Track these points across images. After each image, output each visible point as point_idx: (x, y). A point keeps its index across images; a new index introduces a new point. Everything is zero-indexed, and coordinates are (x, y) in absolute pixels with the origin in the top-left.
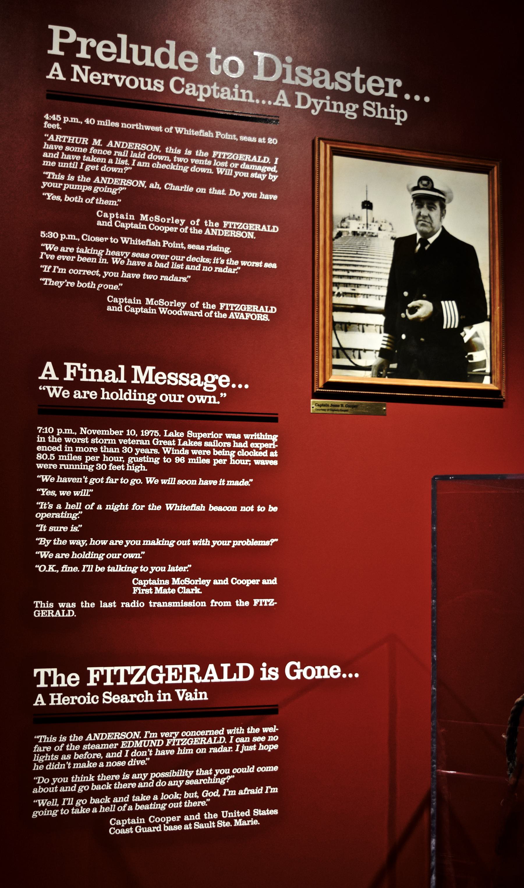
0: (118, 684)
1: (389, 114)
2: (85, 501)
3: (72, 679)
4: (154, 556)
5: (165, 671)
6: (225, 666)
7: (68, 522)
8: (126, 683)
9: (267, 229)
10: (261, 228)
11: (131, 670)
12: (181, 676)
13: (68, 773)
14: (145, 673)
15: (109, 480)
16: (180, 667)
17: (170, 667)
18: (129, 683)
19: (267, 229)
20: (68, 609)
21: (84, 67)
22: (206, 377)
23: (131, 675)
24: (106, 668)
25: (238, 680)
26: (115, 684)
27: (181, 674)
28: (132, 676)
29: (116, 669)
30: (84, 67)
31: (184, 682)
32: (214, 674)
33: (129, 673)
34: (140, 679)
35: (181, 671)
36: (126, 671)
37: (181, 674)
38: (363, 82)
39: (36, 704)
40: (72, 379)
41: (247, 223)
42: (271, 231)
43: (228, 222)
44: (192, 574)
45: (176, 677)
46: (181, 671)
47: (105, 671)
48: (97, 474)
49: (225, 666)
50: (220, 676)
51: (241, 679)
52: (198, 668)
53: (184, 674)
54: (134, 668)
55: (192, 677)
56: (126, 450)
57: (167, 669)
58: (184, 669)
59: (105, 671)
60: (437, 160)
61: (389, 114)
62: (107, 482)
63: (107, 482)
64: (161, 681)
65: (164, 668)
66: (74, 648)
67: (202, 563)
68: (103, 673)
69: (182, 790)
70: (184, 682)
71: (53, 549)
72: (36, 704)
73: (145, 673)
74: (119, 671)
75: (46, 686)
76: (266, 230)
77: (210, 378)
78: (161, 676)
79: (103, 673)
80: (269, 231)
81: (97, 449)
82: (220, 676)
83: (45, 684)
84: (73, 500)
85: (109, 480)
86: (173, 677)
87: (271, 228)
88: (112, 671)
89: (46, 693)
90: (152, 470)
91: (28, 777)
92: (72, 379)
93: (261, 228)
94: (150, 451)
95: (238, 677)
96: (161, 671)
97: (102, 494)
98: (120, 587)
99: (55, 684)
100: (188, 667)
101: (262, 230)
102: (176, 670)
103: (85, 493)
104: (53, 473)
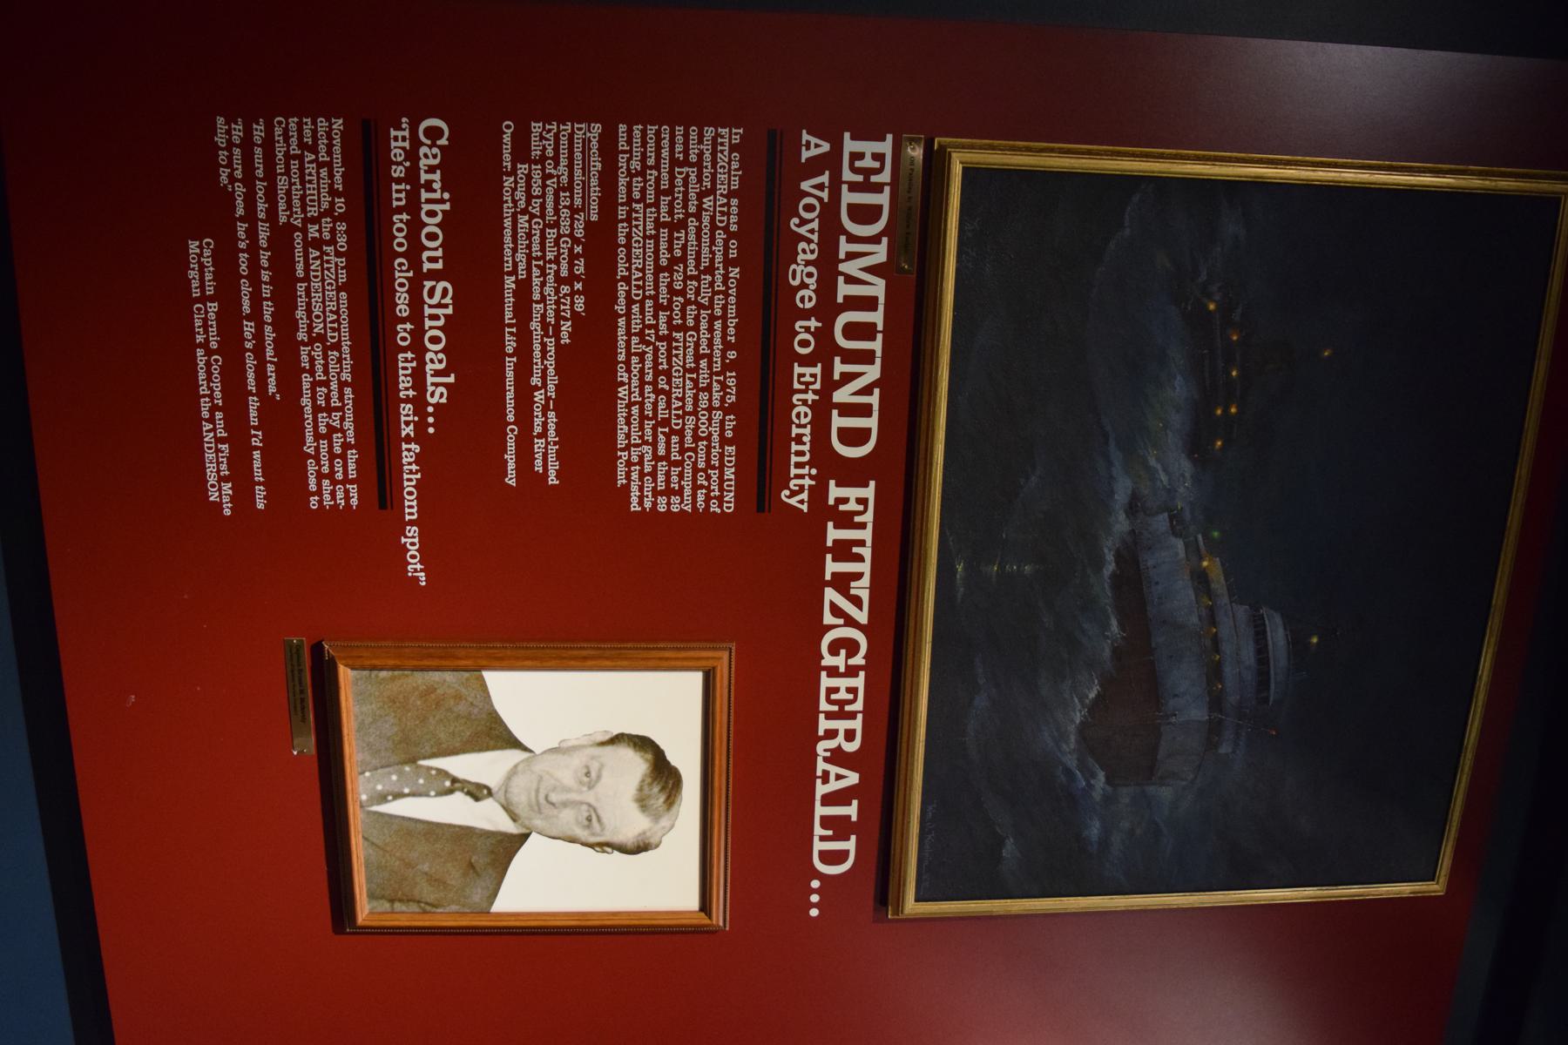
0: (829, 557)
1: (799, 465)
5: (852, 672)
6: (852, 811)
8: (828, 577)
11: (861, 588)
12: (860, 178)
14: (850, 622)
15: (409, 450)
16: (859, 706)
17: (859, 682)
18: (829, 584)
21: (877, 391)
22: (811, 269)
23: (849, 588)
24: (870, 527)
25: (816, 839)
26: (829, 550)
27: (867, 179)
28: (844, 590)
29: (866, 552)
30: (877, 391)
31: (845, 187)
32: (834, 785)
33: (853, 584)
34: (836, 611)
35: (874, 179)
36: (859, 576)
37: (867, 179)
38: (805, 402)
39: (805, 137)
40: (831, 502)
45: (858, 164)
46: (874, 179)
47: (863, 526)
49: (852, 811)
50: (828, 800)
51: (818, 846)
52: (851, 747)
53: (842, 715)
54: (865, 595)
55: (831, 734)
57: (857, 675)
58: (852, 716)
59: (863, 526)
61: (799, 465)
62: (404, 446)
63: (404, 446)
64: (828, 660)
65: (859, 668)
68: (857, 519)
70: (822, 716)
72: (805, 137)
73: (850, 622)
74: (860, 558)
75: (828, 577)
77: (810, 275)
78: (839, 661)
79: (857, 519)
81: (808, 305)
82: (828, 800)
83: (833, 574)
85: (409, 450)
86: (861, 156)
88: (862, 543)
92: (831, 502)
94: (431, 170)
95: (823, 839)
96: (851, 662)
100: (857, 724)
102: (877, 165)
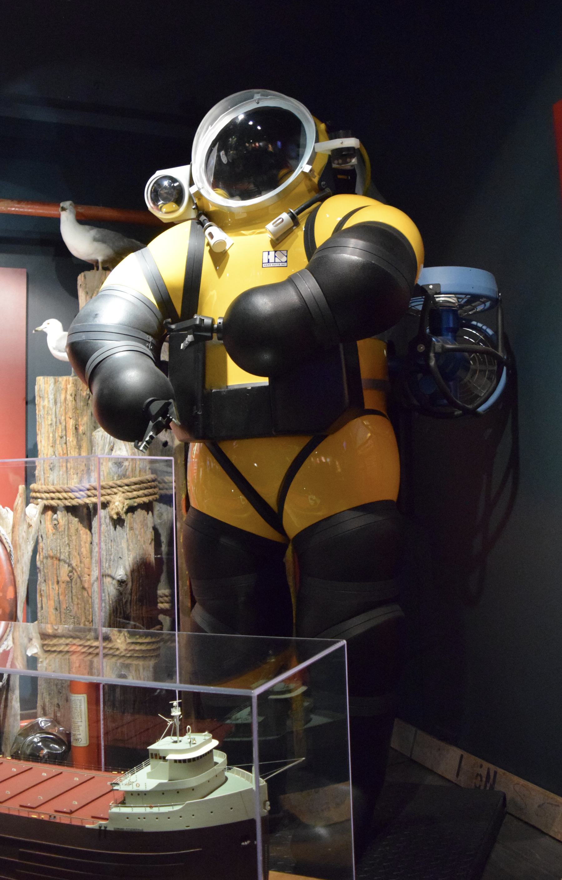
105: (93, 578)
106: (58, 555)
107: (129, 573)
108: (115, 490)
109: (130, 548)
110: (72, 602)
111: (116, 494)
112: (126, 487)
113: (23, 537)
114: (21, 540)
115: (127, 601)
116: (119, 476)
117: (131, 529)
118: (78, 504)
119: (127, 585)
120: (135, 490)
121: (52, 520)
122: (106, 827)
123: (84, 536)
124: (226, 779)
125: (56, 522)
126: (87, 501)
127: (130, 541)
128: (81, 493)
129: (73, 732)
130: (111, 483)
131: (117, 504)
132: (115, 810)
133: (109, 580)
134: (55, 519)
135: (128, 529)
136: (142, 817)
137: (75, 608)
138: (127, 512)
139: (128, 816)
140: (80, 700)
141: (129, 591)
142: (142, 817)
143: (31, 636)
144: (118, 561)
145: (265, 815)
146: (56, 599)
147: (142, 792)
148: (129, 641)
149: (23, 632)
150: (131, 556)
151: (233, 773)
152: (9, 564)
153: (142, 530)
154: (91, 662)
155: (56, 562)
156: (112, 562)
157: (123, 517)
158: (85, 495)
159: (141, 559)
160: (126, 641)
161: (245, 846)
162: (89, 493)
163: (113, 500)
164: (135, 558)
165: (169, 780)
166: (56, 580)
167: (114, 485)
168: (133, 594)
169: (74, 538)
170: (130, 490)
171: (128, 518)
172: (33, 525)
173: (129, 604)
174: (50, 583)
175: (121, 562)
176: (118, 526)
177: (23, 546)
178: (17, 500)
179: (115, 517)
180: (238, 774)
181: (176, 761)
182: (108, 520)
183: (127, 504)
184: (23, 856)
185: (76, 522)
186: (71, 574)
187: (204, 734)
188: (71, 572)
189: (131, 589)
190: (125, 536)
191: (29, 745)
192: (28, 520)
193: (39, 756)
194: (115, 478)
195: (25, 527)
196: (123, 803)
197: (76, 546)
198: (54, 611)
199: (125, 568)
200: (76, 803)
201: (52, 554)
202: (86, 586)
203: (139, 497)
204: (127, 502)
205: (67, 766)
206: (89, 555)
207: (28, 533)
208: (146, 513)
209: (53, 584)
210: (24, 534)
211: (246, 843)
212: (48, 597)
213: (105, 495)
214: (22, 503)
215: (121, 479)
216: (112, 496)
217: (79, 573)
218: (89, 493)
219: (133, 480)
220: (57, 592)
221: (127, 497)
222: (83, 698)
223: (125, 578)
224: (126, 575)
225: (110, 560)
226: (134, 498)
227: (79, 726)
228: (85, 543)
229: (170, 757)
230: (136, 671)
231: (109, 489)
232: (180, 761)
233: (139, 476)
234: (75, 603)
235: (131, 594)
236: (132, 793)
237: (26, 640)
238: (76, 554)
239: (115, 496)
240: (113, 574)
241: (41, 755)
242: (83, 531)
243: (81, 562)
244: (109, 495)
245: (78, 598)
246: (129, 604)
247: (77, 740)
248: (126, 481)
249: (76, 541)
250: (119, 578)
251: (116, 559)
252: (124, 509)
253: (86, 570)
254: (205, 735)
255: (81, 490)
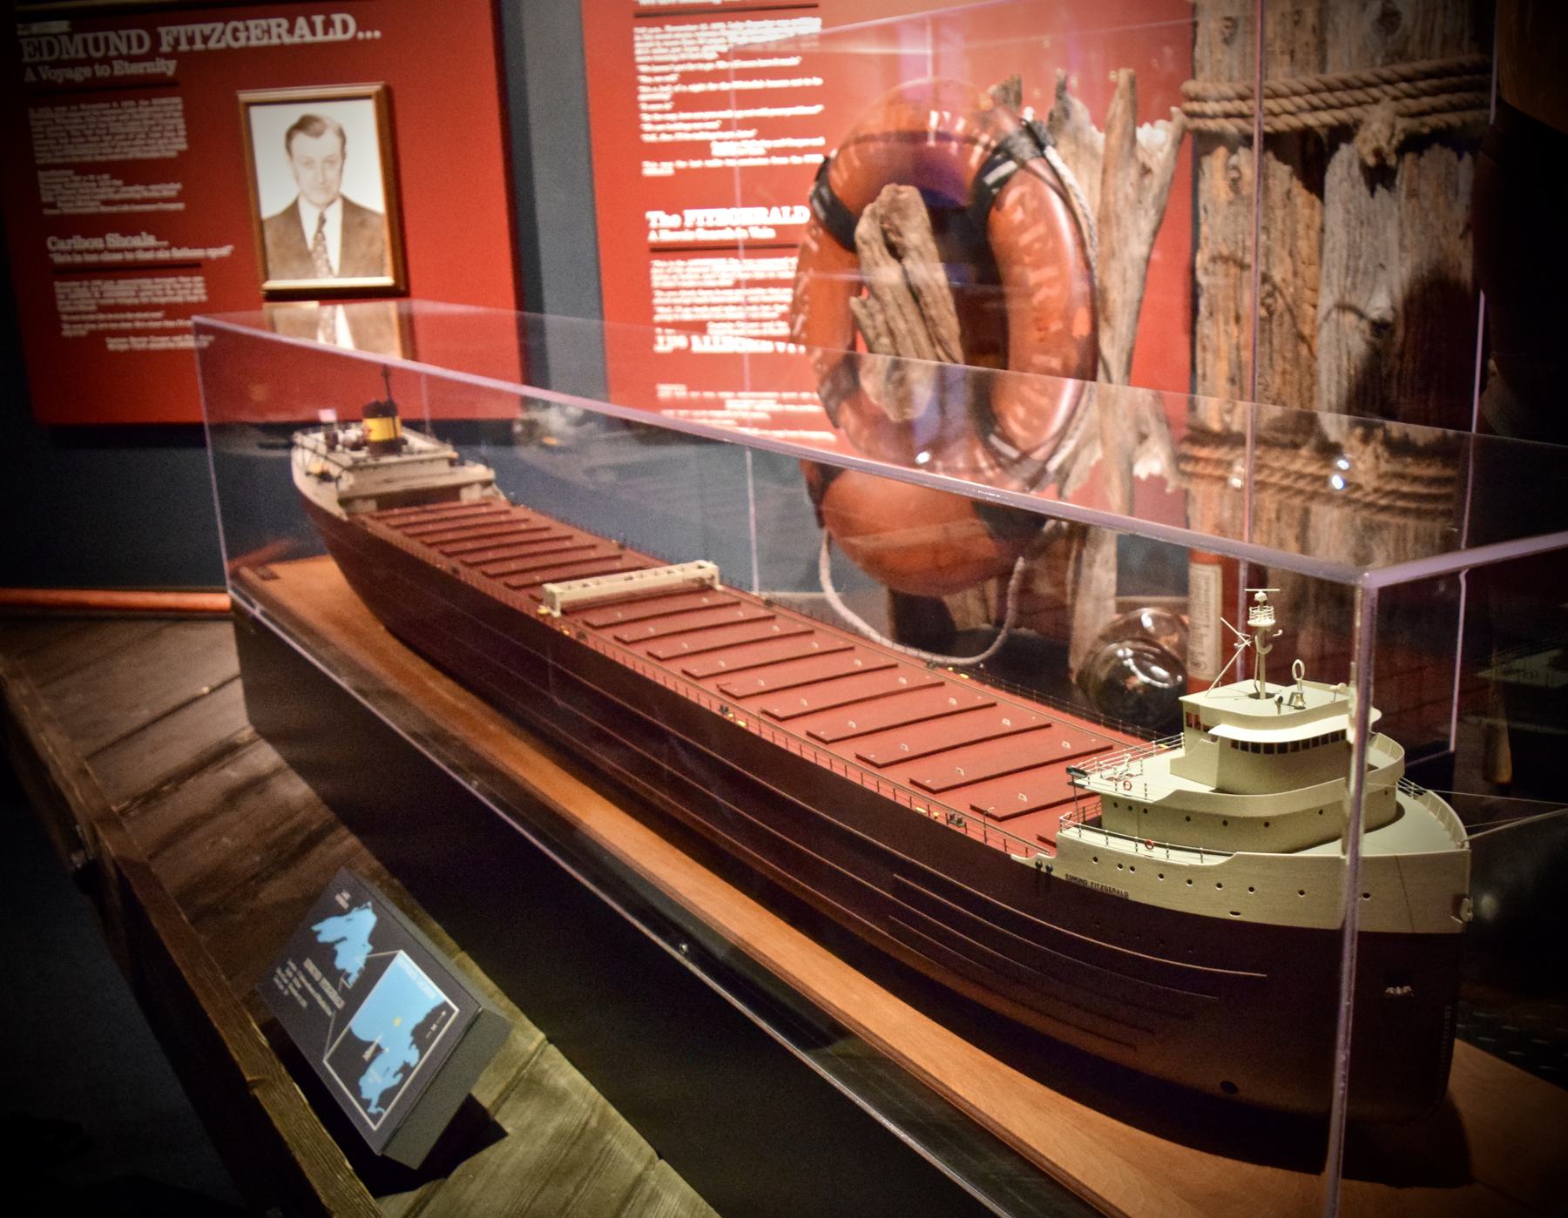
2: (674, 84)
3: (675, 220)
4: (726, 125)
7: (661, 102)
9: (313, 33)
10: (291, 31)
13: (677, 289)
14: (223, 33)
19: (313, 33)
20: (666, 169)
34: (219, 41)
41: (239, 20)
42: (331, 37)
43: (174, 29)
44: (757, 138)
48: (681, 62)
56: (701, 41)
60: (303, 645)
66: (675, 196)
67: (766, 129)
69: (759, 304)
71: (654, 123)
73: (223, 33)
76: (309, 38)
80: (320, 37)
84: (664, 84)
87: (328, 25)
89: (657, 230)
90: (723, 56)
91: (648, 292)
93: (291, 31)
97: (686, 78)
98: (702, 149)
99: (662, 225)
101: (296, 39)
103: (673, 78)
104: (649, 64)
105: (1322, 311)
106: (1240, 254)
107: (1399, 307)
108: (1375, 92)
109: (1407, 242)
110: (1272, 366)
111: (1376, 101)
112: (1404, 86)
113: (1126, 197)
114: (1121, 203)
115: (1389, 375)
116: (1387, 54)
117: (1413, 194)
118: (1287, 129)
119: (1393, 333)
120: (1425, 93)
121: (1228, 168)
122: (1049, 869)
123: (1307, 212)
124: (1400, 812)
125: (1234, 174)
126: (1310, 120)
127: (1407, 224)
128: (1298, 100)
129: (1191, 647)
130: (1366, 75)
131: (1375, 126)
132: (1072, 834)
133: (1350, 318)
134: (1235, 168)
135: (1403, 194)
136: (1127, 865)
137: (1278, 380)
138: (1401, 151)
139: (1096, 855)
140: (1207, 579)
141: (1396, 349)
142: (1127, 865)
143: (1144, 429)
144: (1375, 275)
145: (1458, 931)
146: (1234, 356)
147: (1138, 803)
148: (1384, 467)
149: (1125, 417)
150: (1408, 264)
151: (1425, 803)
152: (1079, 254)
153: (1441, 200)
154: (1306, 512)
155: (1234, 270)
156: (1360, 277)
157: (1392, 161)
158: (1306, 106)
159: (1430, 271)
160: (1377, 467)
161: (1394, 997)
162: (1315, 100)
163: (1367, 118)
164: (1418, 267)
165: (1219, 790)
166: (1232, 314)
167: (1373, 79)
168: (1408, 357)
169: (1279, 213)
170: (1413, 92)
171: (1406, 170)
172: (1156, 169)
173: (1394, 381)
174: (1221, 318)
175: (1382, 276)
176: (1379, 187)
177: (1127, 218)
178: (1113, 106)
179: (1371, 161)
180: (1434, 807)
181: (1235, 744)
182: (1356, 171)
183: (1404, 130)
184: (899, 889)
185: (1286, 177)
186: (1269, 301)
187: (1333, 687)
188: (1270, 295)
189: (1404, 344)
190: (1395, 210)
191: (1106, 662)
192: (1141, 156)
193: (1125, 688)
194: (1379, 61)
195: (1133, 172)
196: (1096, 824)
197: (1283, 234)
198: (1228, 386)
199: (1391, 292)
200: (1025, 799)
201: (1225, 252)
202: (1306, 331)
203: (1435, 110)
204: (1402, 123)
205: (1072, 713)
206: (1315, 258)
207: (1140, 188)
208: (1453, 156)
209: (1227, 323)
210: (1130, 190)
211: (1399, 991)
212: (1217, 352)
213: (1349, 105)
214: (1124, 111)
215: (1393, 62)
216: (1368, 107)
217: (1289, 299)
218: (1315, 100)
219: (1423, 65)
220: (1234, 341)
221: (1405, 110)
222: (1213, 576)
223: (1389, 317)
224: (1393, 309)
225: (1356, 271)
226: (1422, 114)
227: (1202, 636)
228: (1308, 227)
229: (1224, 730)
230: (1397, 541)
231: (1360, 88)
232: (1244, 746)
233: (1442, 56)
234: (1278, 368)
235: (1401, 356)
236: (1114, 802)
237: (1131, 438)
238: (1285, 254)
239: (1374, 108)
240: (1361, 306)
241: (1129, 686)
242: (1301, 196)
243: (1295, 274)
244: (1359, 104)
245: (1284, 358)
246: (1394, 381)
247: (1196, 665)
248: (1404, 68)
249: (1284, 221)
250: (1375, 315)
251: (1371, 269)
252: (1395, 142)
253: (1308, 293)
254: (1335, 692)
255: (1296, 93)
